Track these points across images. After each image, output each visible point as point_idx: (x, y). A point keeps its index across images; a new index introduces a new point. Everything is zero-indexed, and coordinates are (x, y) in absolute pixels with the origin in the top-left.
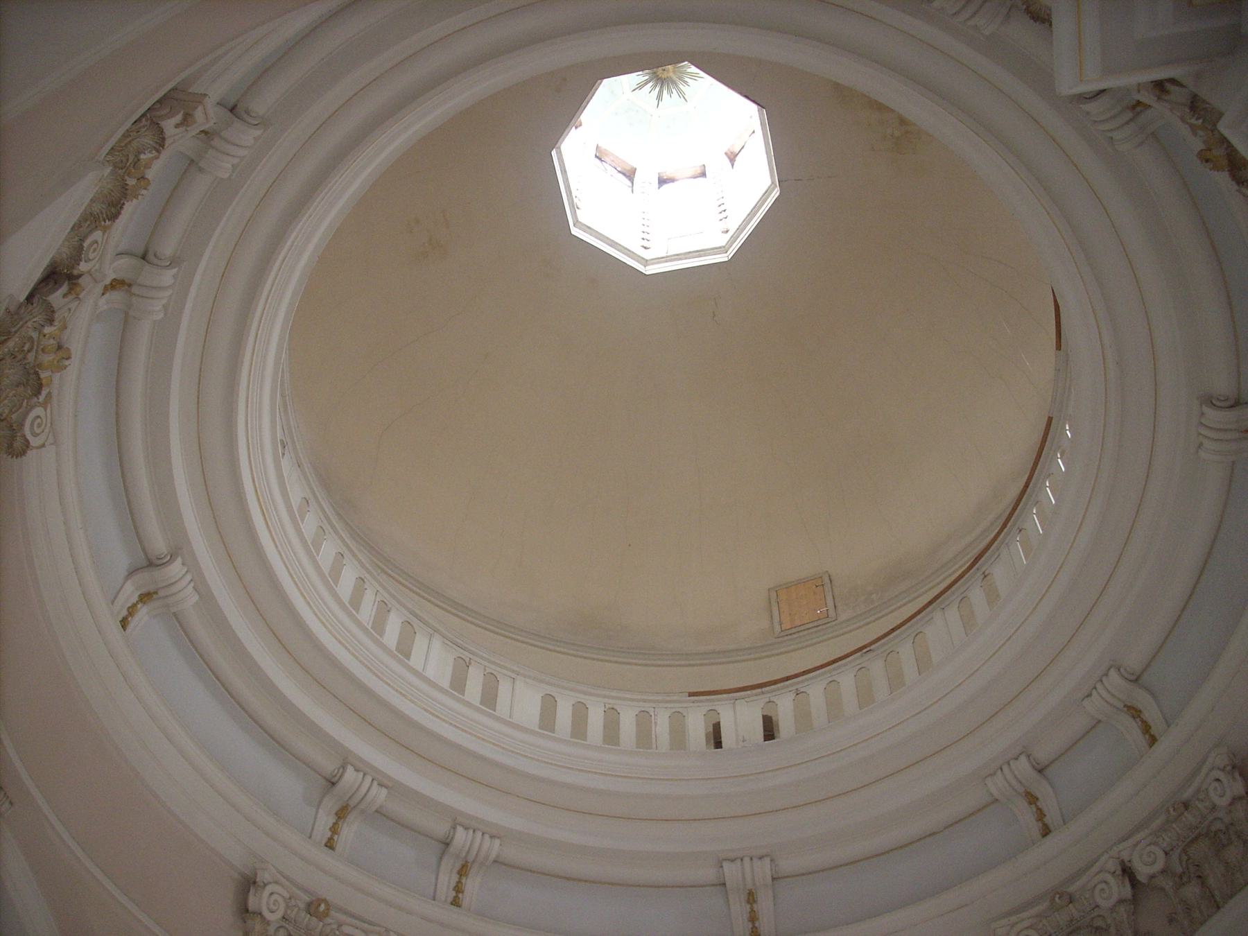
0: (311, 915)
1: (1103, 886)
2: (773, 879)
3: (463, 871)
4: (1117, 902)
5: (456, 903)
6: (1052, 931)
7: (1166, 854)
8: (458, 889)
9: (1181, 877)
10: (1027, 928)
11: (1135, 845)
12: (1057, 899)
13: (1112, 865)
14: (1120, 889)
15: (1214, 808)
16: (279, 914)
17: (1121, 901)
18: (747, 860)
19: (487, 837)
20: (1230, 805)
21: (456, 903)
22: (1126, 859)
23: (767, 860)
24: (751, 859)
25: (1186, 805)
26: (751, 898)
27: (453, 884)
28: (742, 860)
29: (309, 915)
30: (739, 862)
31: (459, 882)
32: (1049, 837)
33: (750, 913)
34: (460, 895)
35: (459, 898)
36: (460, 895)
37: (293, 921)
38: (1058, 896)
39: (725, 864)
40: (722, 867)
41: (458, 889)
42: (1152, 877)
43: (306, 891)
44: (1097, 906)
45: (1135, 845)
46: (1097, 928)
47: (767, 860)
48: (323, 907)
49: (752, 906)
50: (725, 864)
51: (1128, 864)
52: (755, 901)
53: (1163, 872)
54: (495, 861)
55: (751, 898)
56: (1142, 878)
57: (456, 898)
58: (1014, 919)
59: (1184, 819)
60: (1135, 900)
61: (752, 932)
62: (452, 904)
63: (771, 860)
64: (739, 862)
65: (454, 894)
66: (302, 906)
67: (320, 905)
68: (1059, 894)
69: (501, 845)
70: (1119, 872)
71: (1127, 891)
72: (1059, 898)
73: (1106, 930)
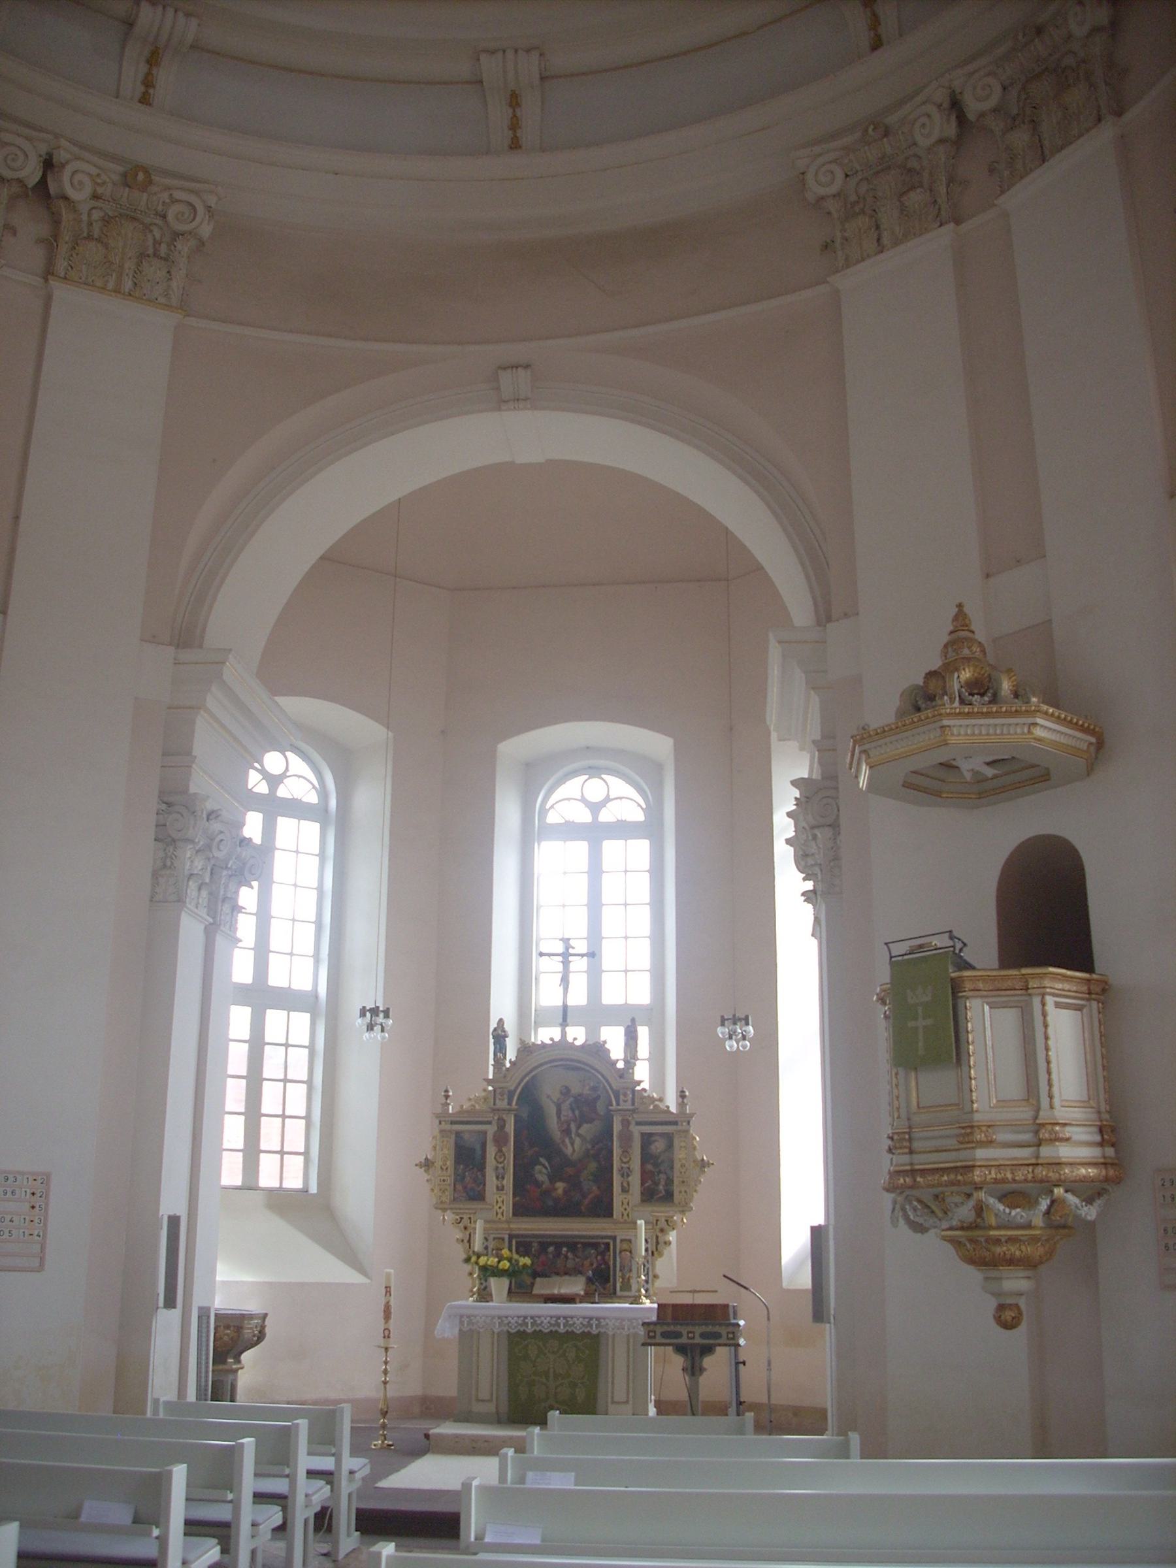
0: (130, 187)
1: (924, 119)
2: (543, 78)
3: (153, 59)
4: (936, 142)
5: (145, 100)
6: (858, 168)
7: (1004, 88)
8: (148, 82)
9: (1014, 119)
10: (830, 162)
11: (971, 74)
12: (870, 130)
13: (941, 96)
14: (943, 126)
15: (1070, 36)
16: (88, 190)
17: (942, 141)
18: (510, 54)
19: (180, 14)
20: (1087, 37)
21: (145, 100)
22: (958, 91)
23: (535, 56)
24: (516, 51)
25: (1039, 31)
26: (514, 100)
27: (141, 77)
28: (504, 51)
29: (127, 189)
30: (500, 54)
31: (149, 74)
32: (877, 53)
33: (512, 118)
34: (151, 91)
35: (150, 94)
36: (151, 91)
37: (110, 199)
38: (872, 127)
39: (484, 58)
40: (479, 60)
41: (148, 82)
42: (982, 115)
43: (114, 158)
44: (915, 144)
45: (971, 74)
46: (910, 170)
47: (535, 56)
48: (141, 176)
49: (514, 111)
50: (484, 58)
51: (958, 97)
52: (518, 105)
53: (995, 110)
54: (192, 47)
55: (514, 100)
56: (971, 116)
57: (145, 93)
58: (817, 149)
59: (1032, 48)
60: (958, 142)
61: (512, 143)
62: (140, 102)
63: (541, 55)
64: (500, 54)
65: (143, 89)
66: (116, 178)
67: (137, 175)
68: (874, 124)
69: (199, 25)
70: (946, 105)
71: (951, 130)
72: (873, 130)
73: (918, 174)
